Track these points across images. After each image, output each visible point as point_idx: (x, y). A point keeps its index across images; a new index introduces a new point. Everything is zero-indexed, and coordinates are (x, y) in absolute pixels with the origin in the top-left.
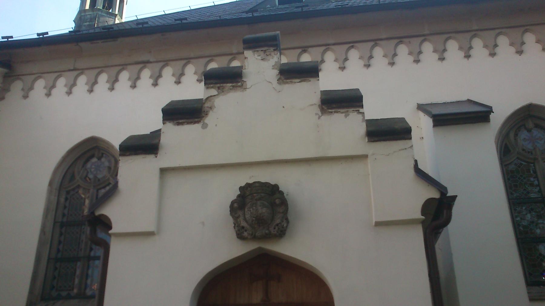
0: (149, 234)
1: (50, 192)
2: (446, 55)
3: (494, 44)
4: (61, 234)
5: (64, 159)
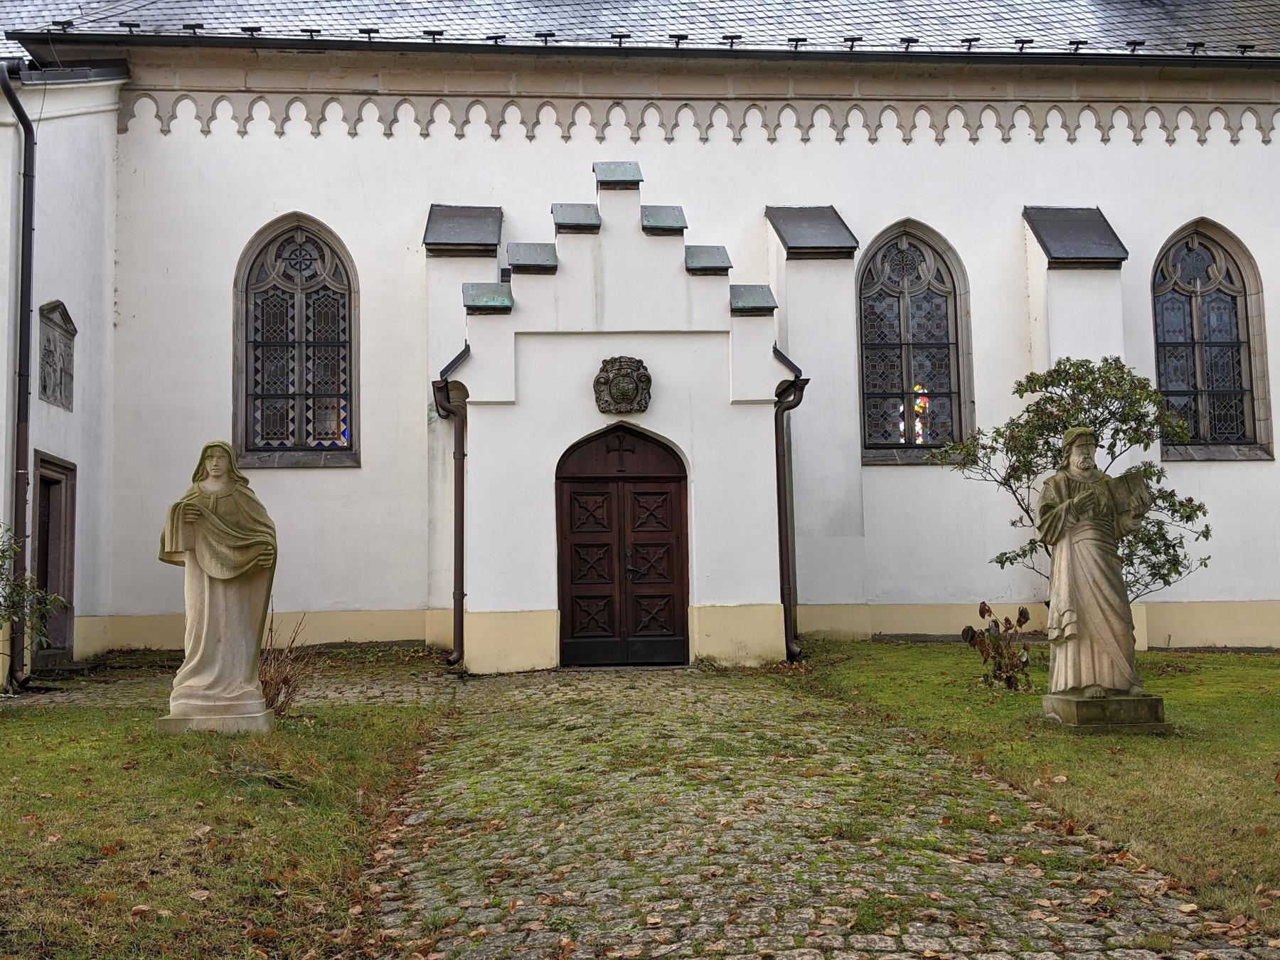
0: (512, 403)
1: (236, 296)
2: (812, 133)
3: (877, 123)
4: (257, 359)
5: (252, 243)
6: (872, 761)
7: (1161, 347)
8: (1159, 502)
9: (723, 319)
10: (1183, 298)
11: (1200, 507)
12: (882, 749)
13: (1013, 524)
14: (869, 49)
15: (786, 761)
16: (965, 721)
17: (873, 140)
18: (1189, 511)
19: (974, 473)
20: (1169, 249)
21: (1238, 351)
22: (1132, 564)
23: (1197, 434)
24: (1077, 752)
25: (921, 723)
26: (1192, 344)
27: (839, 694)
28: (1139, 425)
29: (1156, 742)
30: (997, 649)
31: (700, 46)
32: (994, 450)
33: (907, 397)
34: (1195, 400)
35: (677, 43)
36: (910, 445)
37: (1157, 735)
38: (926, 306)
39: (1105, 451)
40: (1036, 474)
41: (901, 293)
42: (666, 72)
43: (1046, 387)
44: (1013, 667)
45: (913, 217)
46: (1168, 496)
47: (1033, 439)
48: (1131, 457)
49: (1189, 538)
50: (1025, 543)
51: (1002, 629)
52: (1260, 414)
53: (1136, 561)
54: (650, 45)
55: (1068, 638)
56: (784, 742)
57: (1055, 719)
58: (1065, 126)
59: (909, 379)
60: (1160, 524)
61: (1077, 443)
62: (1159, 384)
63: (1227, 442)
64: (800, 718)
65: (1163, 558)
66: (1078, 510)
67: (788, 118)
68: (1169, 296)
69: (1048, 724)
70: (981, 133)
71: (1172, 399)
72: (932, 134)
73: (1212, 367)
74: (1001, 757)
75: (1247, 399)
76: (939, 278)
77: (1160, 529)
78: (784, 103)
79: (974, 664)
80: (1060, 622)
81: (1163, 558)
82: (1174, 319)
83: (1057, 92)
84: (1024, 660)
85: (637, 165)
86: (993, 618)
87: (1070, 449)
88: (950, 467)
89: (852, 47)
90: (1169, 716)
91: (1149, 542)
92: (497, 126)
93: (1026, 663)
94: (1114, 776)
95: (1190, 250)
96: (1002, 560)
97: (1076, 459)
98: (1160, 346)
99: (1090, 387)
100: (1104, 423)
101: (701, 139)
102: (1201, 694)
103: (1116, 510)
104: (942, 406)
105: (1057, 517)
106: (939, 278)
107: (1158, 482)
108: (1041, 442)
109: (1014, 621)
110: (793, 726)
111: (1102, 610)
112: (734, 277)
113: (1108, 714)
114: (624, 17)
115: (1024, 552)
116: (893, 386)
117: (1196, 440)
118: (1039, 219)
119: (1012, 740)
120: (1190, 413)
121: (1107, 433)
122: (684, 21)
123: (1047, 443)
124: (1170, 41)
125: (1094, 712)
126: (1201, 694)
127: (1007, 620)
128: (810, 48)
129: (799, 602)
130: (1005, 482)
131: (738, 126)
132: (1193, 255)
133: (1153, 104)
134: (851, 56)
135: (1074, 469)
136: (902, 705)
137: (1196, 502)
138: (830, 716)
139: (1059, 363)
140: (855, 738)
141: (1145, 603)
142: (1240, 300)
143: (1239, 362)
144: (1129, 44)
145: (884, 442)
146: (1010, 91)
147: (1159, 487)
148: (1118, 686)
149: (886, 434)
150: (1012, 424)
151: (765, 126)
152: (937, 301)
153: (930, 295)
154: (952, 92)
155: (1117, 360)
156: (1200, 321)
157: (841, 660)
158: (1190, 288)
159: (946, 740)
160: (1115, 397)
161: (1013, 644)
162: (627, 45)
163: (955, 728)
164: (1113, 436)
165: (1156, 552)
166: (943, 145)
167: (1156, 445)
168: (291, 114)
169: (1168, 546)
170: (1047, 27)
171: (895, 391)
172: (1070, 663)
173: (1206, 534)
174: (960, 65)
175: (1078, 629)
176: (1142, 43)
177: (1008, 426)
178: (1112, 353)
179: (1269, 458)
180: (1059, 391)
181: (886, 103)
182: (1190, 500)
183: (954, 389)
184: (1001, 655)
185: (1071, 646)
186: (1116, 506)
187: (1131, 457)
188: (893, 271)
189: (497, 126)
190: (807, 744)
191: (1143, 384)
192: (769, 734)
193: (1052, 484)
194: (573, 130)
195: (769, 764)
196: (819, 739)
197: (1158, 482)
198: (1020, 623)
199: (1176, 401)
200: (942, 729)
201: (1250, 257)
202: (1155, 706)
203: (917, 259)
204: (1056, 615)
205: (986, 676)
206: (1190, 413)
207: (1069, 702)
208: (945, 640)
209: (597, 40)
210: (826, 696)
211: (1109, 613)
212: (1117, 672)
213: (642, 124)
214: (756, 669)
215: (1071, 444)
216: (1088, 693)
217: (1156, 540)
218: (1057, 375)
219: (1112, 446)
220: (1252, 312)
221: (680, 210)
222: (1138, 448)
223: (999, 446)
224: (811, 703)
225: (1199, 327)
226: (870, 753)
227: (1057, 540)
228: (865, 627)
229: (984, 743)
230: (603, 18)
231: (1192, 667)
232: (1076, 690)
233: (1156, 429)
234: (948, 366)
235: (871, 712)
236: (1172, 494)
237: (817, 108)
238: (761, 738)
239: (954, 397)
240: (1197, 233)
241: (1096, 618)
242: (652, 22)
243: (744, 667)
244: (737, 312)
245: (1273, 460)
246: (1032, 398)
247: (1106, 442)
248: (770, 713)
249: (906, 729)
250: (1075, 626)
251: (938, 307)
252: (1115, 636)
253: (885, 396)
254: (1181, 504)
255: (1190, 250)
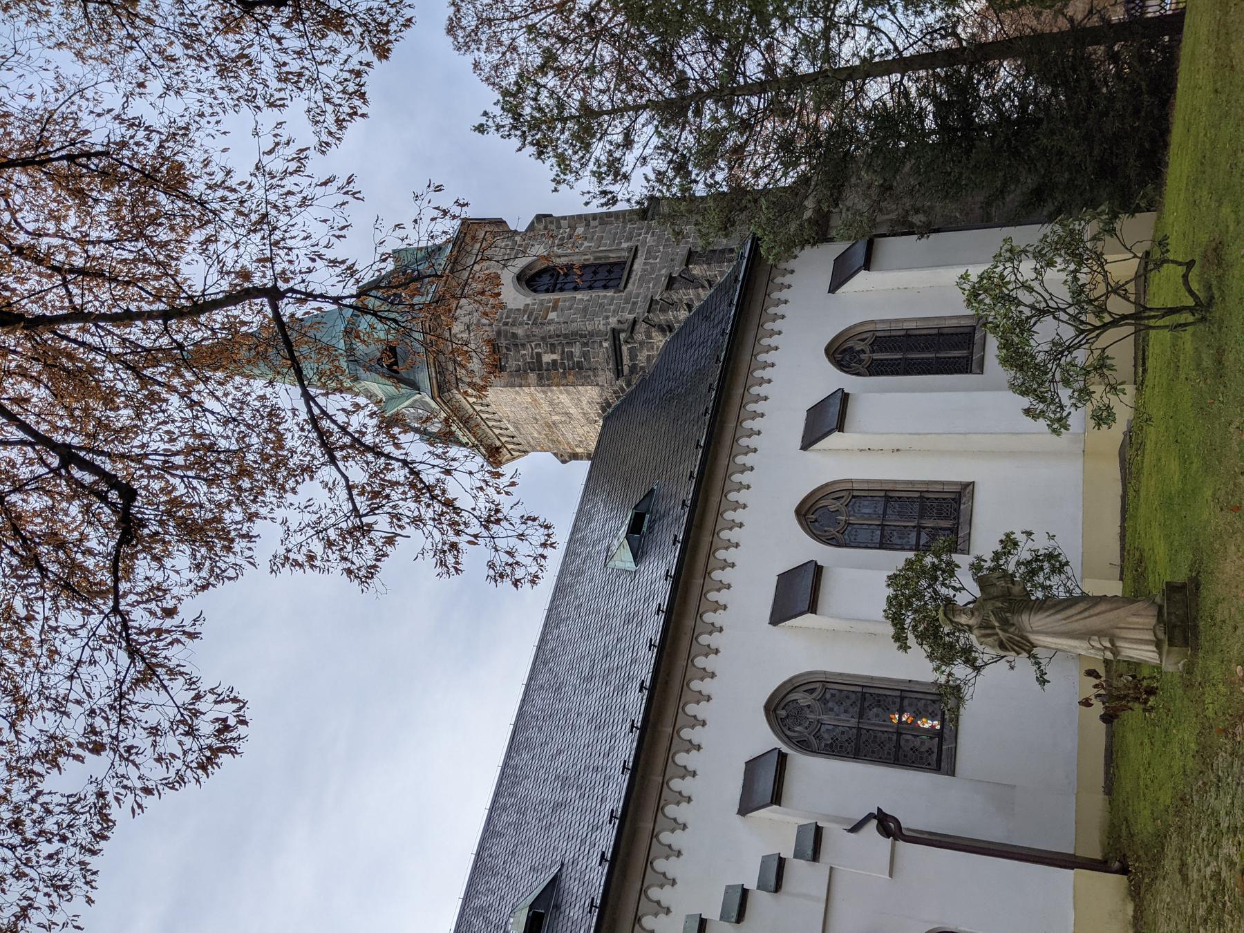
6: (1226, 825)
7: (883, 545)
8: (1001, 562)
9: (821, 869)
10: (849, 528)
11: (1008, 535)
12: (1215, 813)
13: (1012, 668)
14: (641, 716)
15: (1229, 904)
16: (1186, 736)
17: (694, 774)
18: (1009, 543)
19: (967, 692)
20: (788, 737)
21: (892, 497)
22: (1051, 587)
23: (949, 529)
24: (1214, 653)
25: (1188, 772)
26: (883, 526)
27: (1161, 838)
28: (940, 569)
29: (1204, 592)
30: (1119, 698)
31: (612, 843)
32: (950, 674)
33: (900, 730)
34: (924, 528)
35: (606, 860)
36: (940, 735)
37: (1197, 589)
38: (830, 705)
39: (958, 594)
40: (972, 646)
41: (818, 721)
42: (624, 875)
43: (904, 629)
44: (1136, 687)
45: (763, 703)
46: (997, 556)
47: (944, 644)
48: (965, 577)
49: (1030, 544)
50: (1029, 662)
51: (1102, 692)
52: (939, 488)
53: (1048, 583)
54: (602, 884)
55: (1113, 645)
56: (1210, 900)
57: (1184, 664)
58: (719, 590)
59: (887, 726)
60: (1018, 564)
61: (951, 617)
62: (910, 550)
63: (958, 511)
64: (1185, 879)
65: (1046, 565)
66: (1005, 624)
67: (676, 784)
68: (846, 537)
69: (1189, 669)
70: (713, 646)
71: (922, 543)
72: (708, 680)
73: (902, 515)
74: (1220, 714)
75: (927, 495)
76: (811, 691)
77: (1023, 563)
78: (665, 785)
79: (1133, 717)
80: (1099, 649)
81: (1046, 565)
82: (863, 536)
83: (728, 438)
84: (1130, 678)
85: (688, 916)
86: (1093, 697)
87: (956, 623)
88: (962, 709)
89: (637, 728)
90: (1181, 577)
91: (1033, 573)
92: (719, 607)
93: (1134, 677)
94: (1235, 628)
95: (816, 521)
96: (1042, 680)
97: (963, 620)
98: (882, 546)
99: (908, 599)
100: (935, 591)
101: (678, 856)
102: (1161, 550)
103: (1007, 596)
104: (910, 705)
105: (1010, 640)
106: (811, 691)
107: (986, 561)
108: (947, 638)
109: (1097, 681)
110: (1193, 886)
111: (1089, 617)
112: (788, 853)
113: (1179, 623)
114: (579, 899)
115: (1036, 663)
116: (890, 739)
117: (954, 530)
118: (779, 616)
119: (1204, 701)
120: (934, 533)
121: (944, 591)
122: (592, 851)
123: (948, 635)
124: (678, 519)
125: (1177, 632)
126: (1161, 550)
127: (1096, 686)
128: (631, 759)
129: (1071, 852)
130: (977, 669)
131: (679, 798)
132: (819, 519)
133: (715, 533)
134: (643, 729)
135: (972, 622)
136: (1171, 785)
137: (1003, 538)
138: (1182, 850)
139: (887, 618)
140: (1204, 833)
141: (1082, 578)
142: (855, 493)
143: (899, 498)
144: (674, 544)
145: (936, 754)
146: (689, 623)
147: (989, 561)
148: (1156, 613)
149: (930, 751)
150: (931, 657)
151: (678, 803)
152: (828, 696)
153: (823, 700)
154: (731, 425)
155: (889, 578)
156: (867, 519)
157: (1128, 827)
158: (842, 523)
159: (1205, 754)
160: (917, 583)
161: (1115, 683)
162: (599, 902)
163: (1193, 745)
164: (947, 587)
165: (1041, 568)
166: (717, 673)
167: (956, 558)
168: (655, 899)
169: (1037, 559)
170: (652, 593)
171: (895, 738)
172: (1135, 646)
173: (1029, 534)
174: (665, 654)
175: (1105, 636)
176: (676, 536)
177: (932, 660)
178: (883, 581)
179: (971, 486)
180: (908, 621)
181: (680, 710)
182: (1001, 541)
183: (898, 693)
184: (1126, 696)
185: (1119, 644)
186: (1002, 596)
187: (965, 577)
188: (800, 725)
189: (719, 607)
190: (1211, 879)
191: (909, 563)
192: (1201, 912)
193: (982, 639)
194: (685, 794)
195: (1233, 921)
196: (1206, 867)
197: (986, 561)
198: (1098, 676)
199: (924, 539)
200: (1193, 756)
201: (827, 485)
202: (1172, 589)
203: (795, 705)
204: (1092, 651)
205: (1145, 710)
206: (934, 533)
207: (1168, 652)
208: (1110, 736)
209: (590, 926)
210: (1163, 849)
211: (1092, 612)
212: (1143, 613)
213: (658, 902)
214: (1136, 906)
215: (951, 622)
216: (1161, 636)
217: (1032, 567)
218: (896, 619)
219: (954, 588)
220: (865, 487)
221: (728, 887)
222: (958, 572)
223: (948, 670)
224: (1170, 864)
225: (872, 520)
226: (1218, 824)
227: (1029, 641)
228: (1098, 799)
229: (1207, 725)
230: (576, 917)
231: (1137, 554)
232: (1158, 644)
233: (944, 557)
234: (879, 695)
235: (1177, 812)
236: (996, 553)
237: (673, 761)
238: (1206, 921)
239: (905, 694)
240: (805, 516)
241: (1096, 622)
242: (587, 878)
243: (1134, 917)
244: (815, 857)
245: (974, 482)
246: (912, 640)
247: (952, 593)
248: (1179, 905)
249: (1194, 787)
250: (1102, 639)
251: (833, 695)
252: (1112, 610)
253: (898, 746)
254: (1004, 548)
255: (816, 521)
